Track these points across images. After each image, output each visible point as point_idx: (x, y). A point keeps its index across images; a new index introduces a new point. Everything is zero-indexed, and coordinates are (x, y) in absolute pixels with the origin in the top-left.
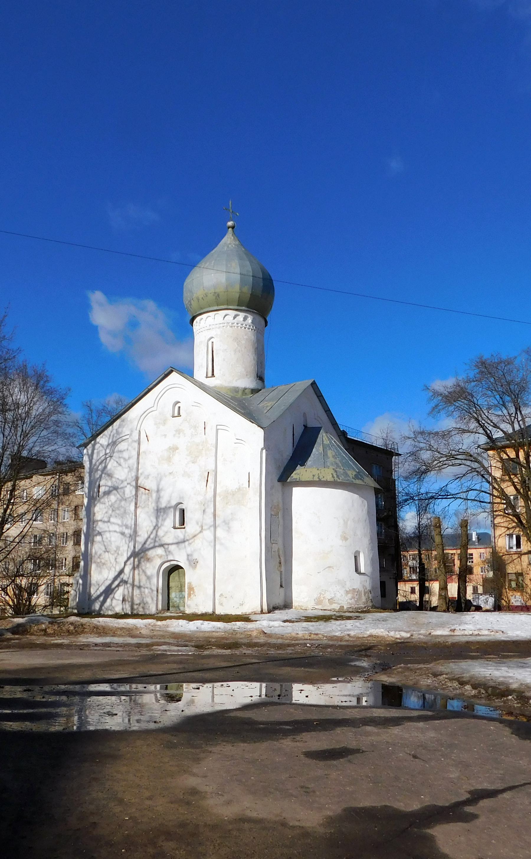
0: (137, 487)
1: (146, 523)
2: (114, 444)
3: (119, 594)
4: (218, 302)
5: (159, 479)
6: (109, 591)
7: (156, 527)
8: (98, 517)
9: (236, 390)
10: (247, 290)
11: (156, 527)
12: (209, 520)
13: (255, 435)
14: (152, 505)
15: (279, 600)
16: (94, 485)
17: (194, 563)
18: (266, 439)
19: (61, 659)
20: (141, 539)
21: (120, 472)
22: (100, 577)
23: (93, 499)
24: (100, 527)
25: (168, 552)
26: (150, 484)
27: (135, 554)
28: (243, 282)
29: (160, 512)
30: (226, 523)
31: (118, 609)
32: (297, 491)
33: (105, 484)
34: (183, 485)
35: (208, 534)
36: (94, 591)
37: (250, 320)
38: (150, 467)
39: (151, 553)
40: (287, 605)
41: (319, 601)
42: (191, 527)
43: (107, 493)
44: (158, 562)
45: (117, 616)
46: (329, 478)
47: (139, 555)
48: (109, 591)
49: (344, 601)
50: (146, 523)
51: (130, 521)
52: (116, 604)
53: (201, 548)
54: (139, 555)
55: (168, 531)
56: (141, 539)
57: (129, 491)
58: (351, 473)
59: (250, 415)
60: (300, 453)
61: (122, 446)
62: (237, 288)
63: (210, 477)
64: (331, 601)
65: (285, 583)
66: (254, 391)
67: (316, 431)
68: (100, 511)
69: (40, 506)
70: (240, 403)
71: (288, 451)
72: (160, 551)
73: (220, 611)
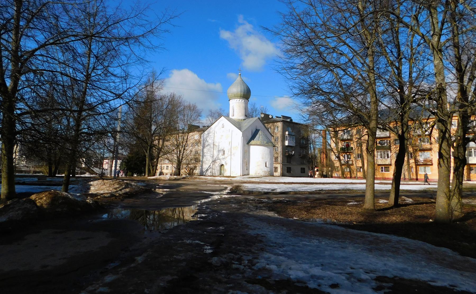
0: (214, 145)
1: (216, 153)
2: (209, 134)
3: (209, 171)
4: (235, 97)
5: (219, 143)
6: (207, 170)
7: (218, 155)
8: (205, 152)
9: (239, 120)
10: (242, 93)
11: (218, 155)
12: (230, 153)
13: (240, 133)
14: (217, 149)
15: (246, 173)
16: (204, 144)
17: (226, 164)
18: (243, 134)
19: (363, 234)
20: (214, 158)
21: (210, 141)
22: (205, 167)
23: (204, 147)
24: (205, 154)
25: (221, 161)
26: (217, 144)
27: (213, 161)
28: (241, 91)
29: (219, 151)
30: (234, 154)
31: (209, 175)
32: (251, 146)
33: (206, 144)
34: (224, 145)
35: (230, 157)
36: (204, 170)
37: (243, 101)
38: (217, 140)
39: (217, 161)
40: (248, 175)
41: (256, 174)
42: (226, 155)
43: (207, 146)
44: (218, 163)
45: (226, 177)
46: (259, 144)
47: (214, 161)
48: (207, 170)
49: (262, 174)
50: (216, 153)
51: (212, 153)
52: (209, 173)
53: (228, 160)
54: (214, 161)
55: (221, 157)
56: (214, 158)
57: (212, 146)
58: (265, 142)
59: (240, 129)
60: (253, 137)
61: (211, 134)
62: (239, 93)
63: (230, 143)
64: (259, 174)
65: (248, 169)
66: (244, 120)
67: (259, 130)
68: (205, 150)
69: (121, 190)
70: (238, 124)
71: (250, 136)
72: (219, 161)
73: (232, 176)
